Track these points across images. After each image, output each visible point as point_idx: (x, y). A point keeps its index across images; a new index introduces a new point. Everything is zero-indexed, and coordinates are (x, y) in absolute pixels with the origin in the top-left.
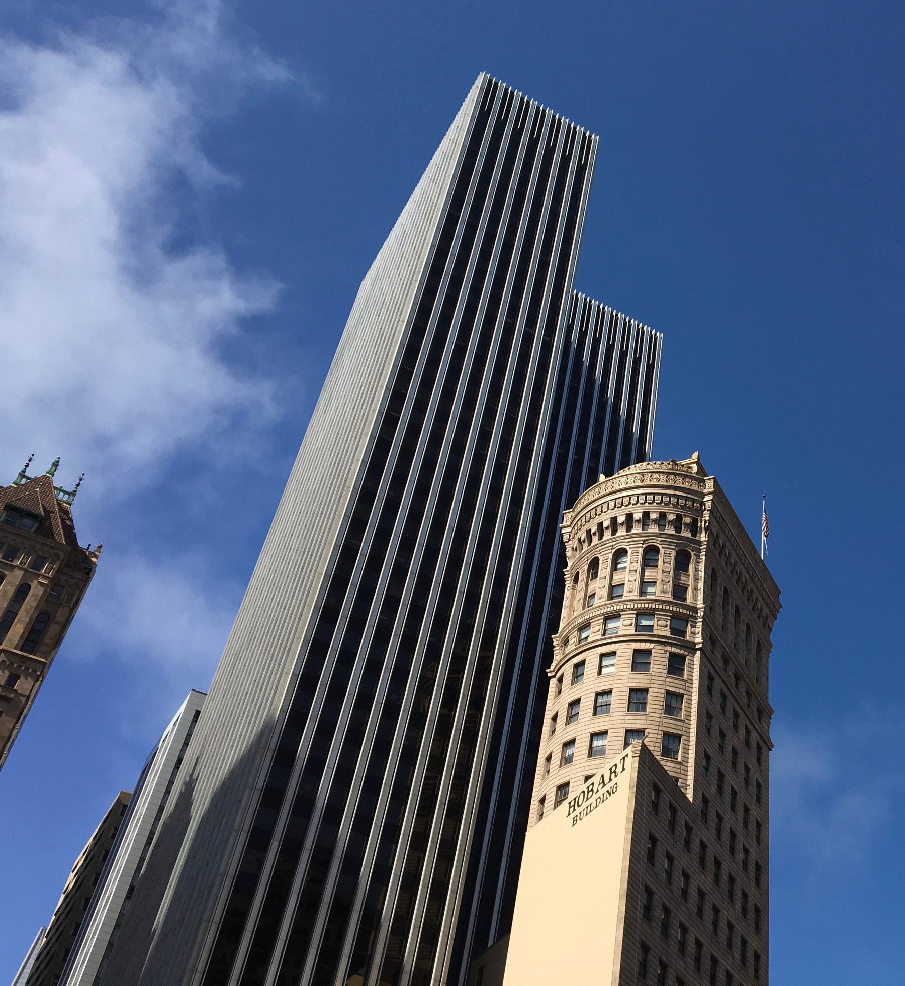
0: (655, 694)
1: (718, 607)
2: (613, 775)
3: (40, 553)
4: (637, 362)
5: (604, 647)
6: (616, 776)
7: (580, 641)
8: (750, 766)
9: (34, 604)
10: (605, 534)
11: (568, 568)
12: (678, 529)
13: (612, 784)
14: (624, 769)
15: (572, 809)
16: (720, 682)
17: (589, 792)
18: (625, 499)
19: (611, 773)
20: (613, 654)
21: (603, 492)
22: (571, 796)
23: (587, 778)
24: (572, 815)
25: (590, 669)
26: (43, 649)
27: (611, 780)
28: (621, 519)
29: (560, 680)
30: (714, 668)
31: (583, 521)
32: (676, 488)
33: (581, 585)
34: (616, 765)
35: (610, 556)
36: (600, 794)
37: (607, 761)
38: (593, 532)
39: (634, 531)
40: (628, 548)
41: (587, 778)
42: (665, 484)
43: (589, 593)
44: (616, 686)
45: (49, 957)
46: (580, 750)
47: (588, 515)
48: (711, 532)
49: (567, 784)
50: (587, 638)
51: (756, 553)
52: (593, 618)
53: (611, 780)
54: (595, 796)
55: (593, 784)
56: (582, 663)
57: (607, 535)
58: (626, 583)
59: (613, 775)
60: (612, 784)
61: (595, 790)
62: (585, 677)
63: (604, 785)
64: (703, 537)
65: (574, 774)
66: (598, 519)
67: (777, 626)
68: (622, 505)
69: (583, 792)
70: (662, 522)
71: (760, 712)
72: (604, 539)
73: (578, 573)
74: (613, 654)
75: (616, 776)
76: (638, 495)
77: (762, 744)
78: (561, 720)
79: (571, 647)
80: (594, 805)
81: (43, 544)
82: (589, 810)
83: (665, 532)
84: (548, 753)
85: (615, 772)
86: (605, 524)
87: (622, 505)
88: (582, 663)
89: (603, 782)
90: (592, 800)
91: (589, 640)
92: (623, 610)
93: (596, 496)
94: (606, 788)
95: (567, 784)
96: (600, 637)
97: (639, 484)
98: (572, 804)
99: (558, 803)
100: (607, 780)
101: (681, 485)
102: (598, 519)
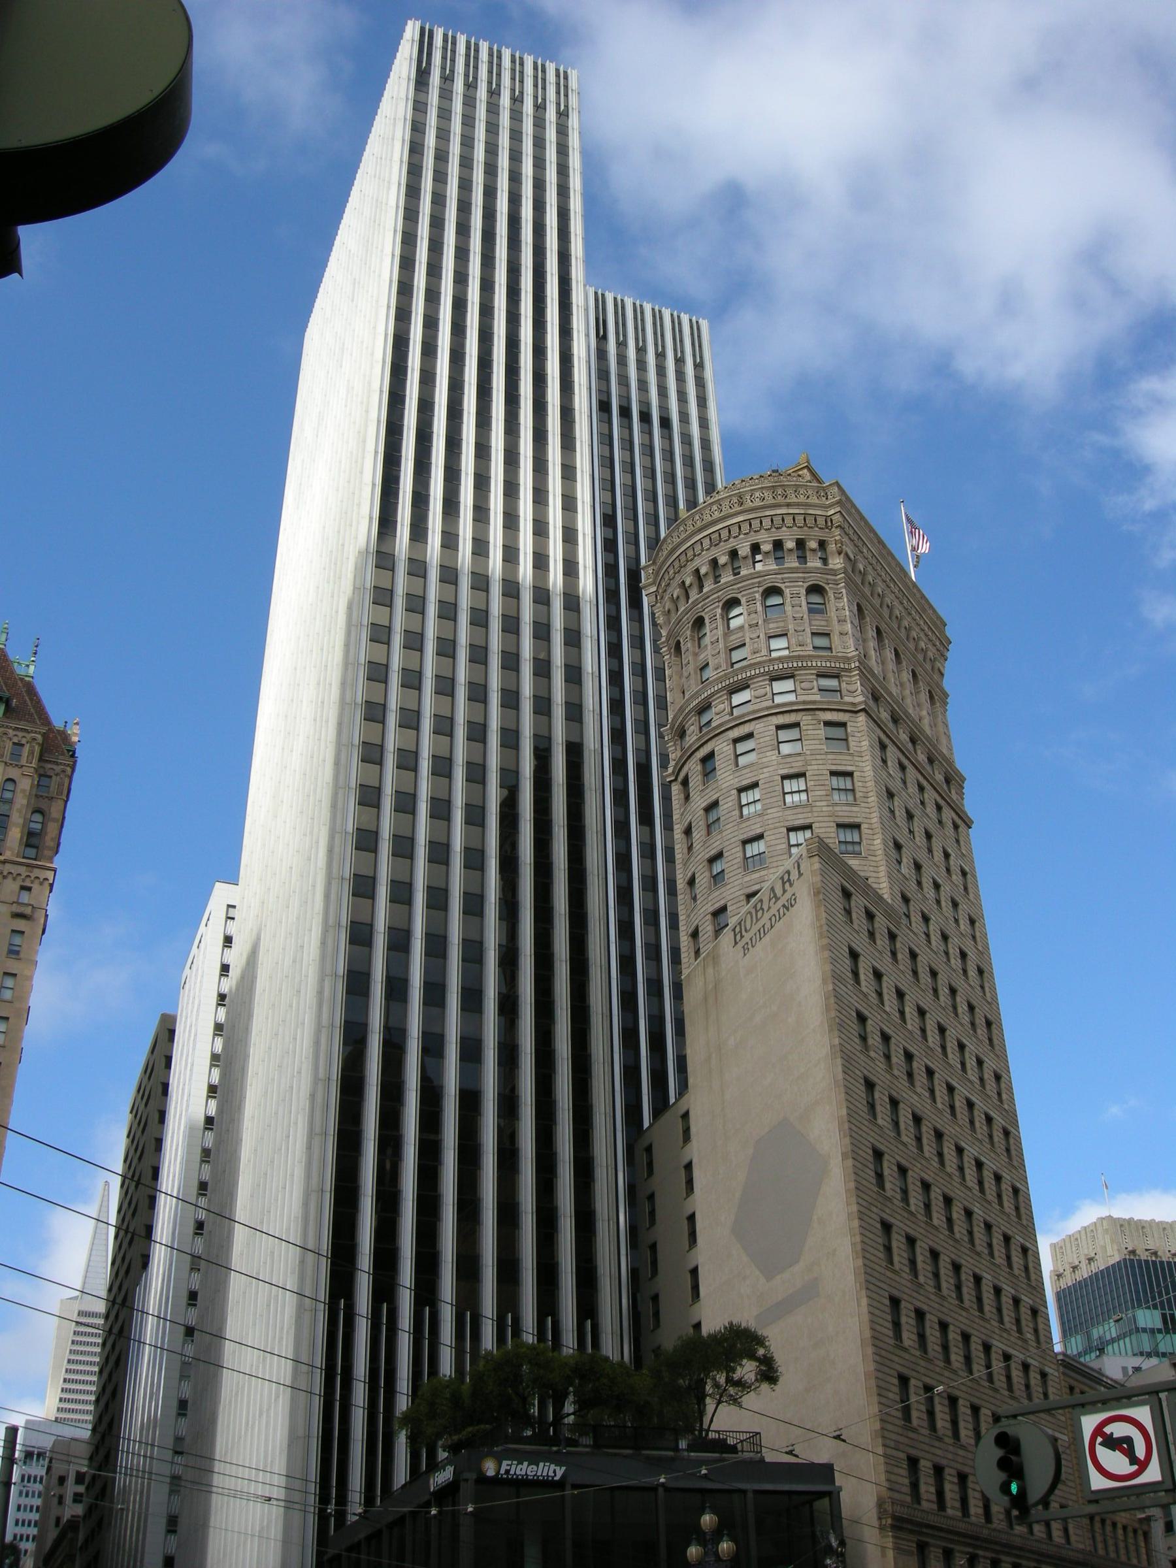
0: (816, 778)
1: (873, 652)
2: (787, 885)
3: (15, 740)
4: (680, 361)
5: (736, 729)
6: (791, 885)
7: (701, 728)
8: (950, 851)
9: (25, 802)
10: (691, 595)
11: (663, 639)
12: (803, 559)
13: (788, 895)
14: (800, 874)
15: (738, 937)
16: (895, 749)
17: (757, 912)
18: (722, 532)
19: (784, 883)
20: (750, 736)
21: (690, 529)
22: (732, 921)
23: (749, 896)
24: (741, 944)
25: (722, 763)
26: (47, 853)
27: (785, 891)
28: (723, 560)
29: (685, 783)
30: (885, 732)
31: (671, 572)
32: (788, 505)
33: (687, 657)
34: (788, 872)
35: (719, 611)
36: (774, 911)
37: (772, 871)
38: (687, 583)
39: (744, 572)
40: (739, 596)
41: (749, 896)
42: (773, 501)
43: (700, 664)
44: (761, 776)
45: (133, 1206)
46: (731, 862)
47: (677, 564)
48: (847, 554)
49: (724, 909)
50: (710, 721)
51: (906, 574)
52: (713, 695)
53: (785, 891)
54: (767, 916)
55: (761, 901)
56: (711, 755)
57: (708, 586)
58: (747, 640)
59: (787, 885)
60: (788, 895)
61: (765, 907)
62: (718, 773)
63: (777, 899)
64: (836, 562)
65: (731, 893)
66: (691, 567)
67: (949, 668)
68: (720, 540)
69: (750, 913)
70: (779, 554)
71: (948, 781)
72: (705, 590)
73: (678, 643)
74: (750, 736)
75: (791, 885)
76: (739, 524)
77: (959, 822)
78: (698, 835)
79: (691, 738)
80: (768, 926)
81: (16, 729)
82: (762, 932)
83: (786, 565)
84: (690, 875)
85: (789, 880)
86: (703, 571)
87: (720, 540)
88: (711, 755)
89: (775, 896)
90: (765, 920)
91: (714, 724)
92: (751, 677)
93: (683, 536)
94: (780, 903)
95: (724, 909)
96: (727, 718)
97: (737, 508)
98: (738, 930)
99: (718, 932)
100: (779, 892)
101: (795, 500)
102: (691, 567)
